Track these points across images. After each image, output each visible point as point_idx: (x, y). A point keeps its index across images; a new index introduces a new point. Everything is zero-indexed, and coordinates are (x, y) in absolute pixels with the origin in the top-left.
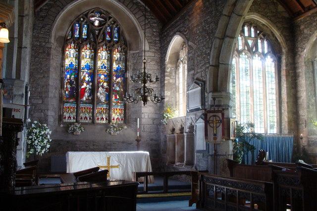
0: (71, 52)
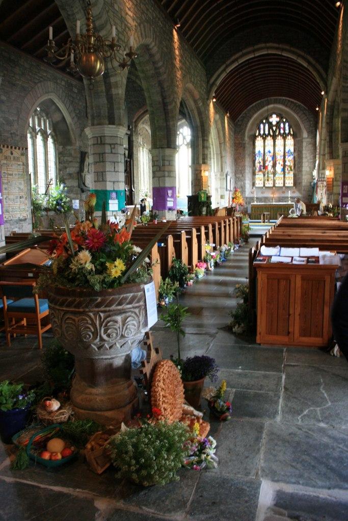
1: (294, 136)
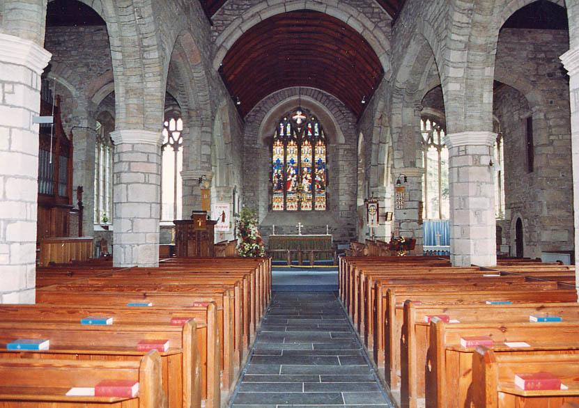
0: (278, 149)
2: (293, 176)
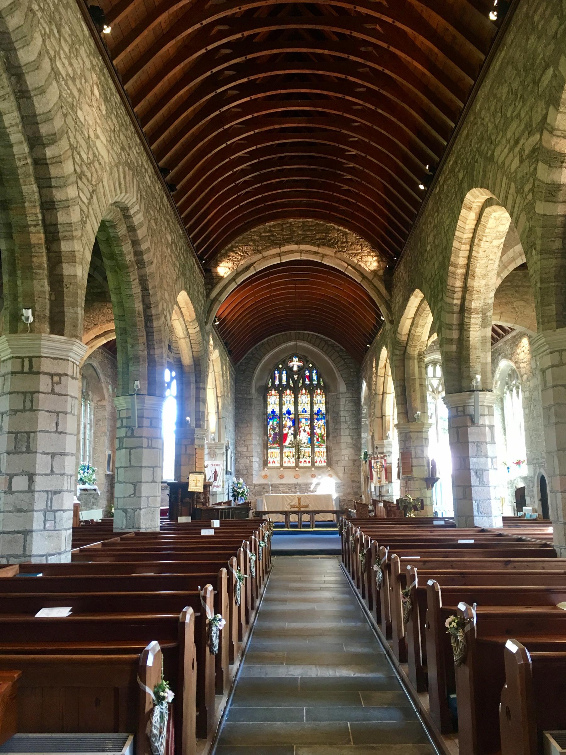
1: (326, 390)
2: (289, 428)
